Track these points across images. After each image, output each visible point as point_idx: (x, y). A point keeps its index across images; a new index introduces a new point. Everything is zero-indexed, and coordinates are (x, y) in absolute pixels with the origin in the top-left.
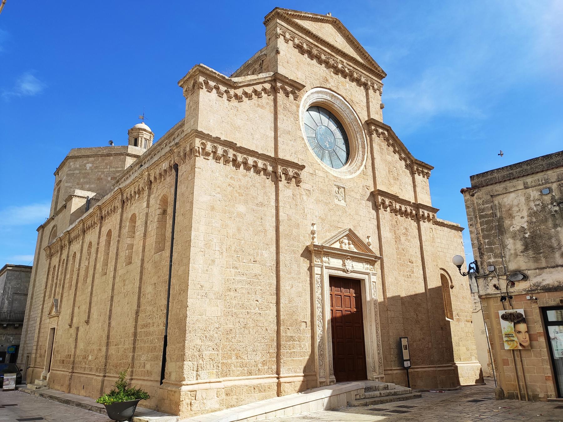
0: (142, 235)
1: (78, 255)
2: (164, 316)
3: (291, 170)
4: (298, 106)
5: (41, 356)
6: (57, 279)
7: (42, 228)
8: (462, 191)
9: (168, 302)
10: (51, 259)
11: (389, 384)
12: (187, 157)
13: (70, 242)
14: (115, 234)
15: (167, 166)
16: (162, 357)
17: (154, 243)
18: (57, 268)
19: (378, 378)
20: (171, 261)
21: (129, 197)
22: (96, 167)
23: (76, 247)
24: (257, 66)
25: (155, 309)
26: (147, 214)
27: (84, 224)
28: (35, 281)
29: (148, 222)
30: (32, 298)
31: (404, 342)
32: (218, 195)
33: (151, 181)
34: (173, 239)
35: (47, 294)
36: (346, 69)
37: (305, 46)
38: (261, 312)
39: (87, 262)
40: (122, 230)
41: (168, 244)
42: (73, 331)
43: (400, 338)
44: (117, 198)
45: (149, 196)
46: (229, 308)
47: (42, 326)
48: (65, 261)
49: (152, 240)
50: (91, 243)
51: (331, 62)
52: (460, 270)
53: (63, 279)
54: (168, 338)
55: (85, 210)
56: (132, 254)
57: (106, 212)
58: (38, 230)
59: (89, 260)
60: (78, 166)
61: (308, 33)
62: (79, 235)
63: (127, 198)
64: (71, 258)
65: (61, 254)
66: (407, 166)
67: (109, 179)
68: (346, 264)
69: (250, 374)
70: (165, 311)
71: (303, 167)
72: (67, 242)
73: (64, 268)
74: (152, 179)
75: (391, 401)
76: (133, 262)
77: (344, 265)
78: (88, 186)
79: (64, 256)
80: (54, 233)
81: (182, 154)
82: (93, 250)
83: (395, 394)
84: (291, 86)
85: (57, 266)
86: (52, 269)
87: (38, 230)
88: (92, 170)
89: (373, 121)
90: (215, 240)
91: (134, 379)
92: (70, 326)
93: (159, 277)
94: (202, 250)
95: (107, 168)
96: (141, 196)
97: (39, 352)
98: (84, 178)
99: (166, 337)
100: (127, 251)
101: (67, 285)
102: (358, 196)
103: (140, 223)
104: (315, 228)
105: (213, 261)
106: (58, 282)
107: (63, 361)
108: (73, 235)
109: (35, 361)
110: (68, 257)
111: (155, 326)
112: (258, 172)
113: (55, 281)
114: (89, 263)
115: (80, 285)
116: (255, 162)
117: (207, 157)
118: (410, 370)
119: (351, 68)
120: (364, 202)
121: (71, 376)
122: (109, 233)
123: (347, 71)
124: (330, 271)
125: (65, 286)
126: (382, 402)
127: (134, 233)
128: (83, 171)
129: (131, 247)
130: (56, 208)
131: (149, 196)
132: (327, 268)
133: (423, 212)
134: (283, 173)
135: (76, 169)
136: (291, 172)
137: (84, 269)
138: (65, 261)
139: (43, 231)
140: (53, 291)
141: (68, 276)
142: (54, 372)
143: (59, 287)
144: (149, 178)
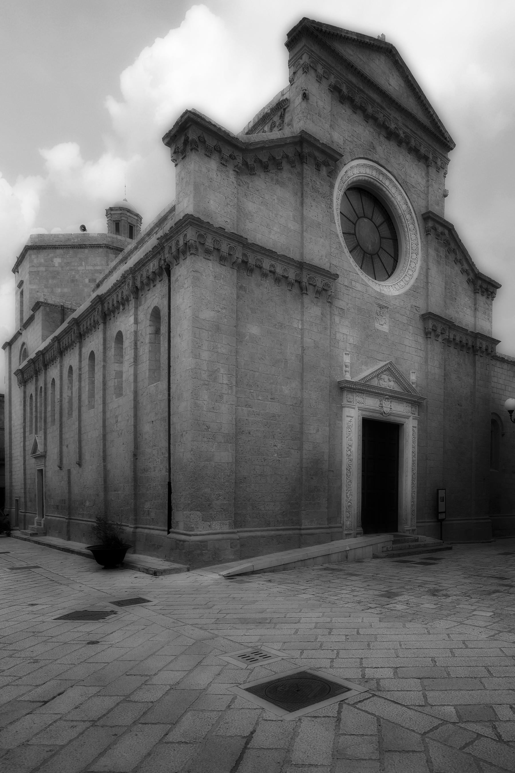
0: (132, 360)
1: (57, 382)
2: (166, 460)
3: (320, 280)
4: (332, 186)
5: (31, 501)
6: (36, 411)
7: (8, 345)
9: (169, 444)
10: (25, 386)
11: (420, 536)
12: (181, 255)
14: (99, 356)
15: (156, 267)
16: (167, 505)
17: (147, 372)
18: (34, 398)
19: (409, 530)
20: (169, 395)
21: (111, 309)
22: (68, 264)
23: (54, 372)
24: (276, 119)
25: (155, 452)
26: (136, 332)
27: (59, 343)
28: (10, 413)
29: (138, 343)
30: (10, 433)
31: (442, 493)
32: (224, 311)
33: (137, 287)
34: (169, 367)
35: (27, 429)
36: (401, 132)
37: (344, 89)
38: (280, 459)
39: (70, 392)
40: (108, 352)
41: (165, 372)
42: (64, 473)
43: (438, 490)
44: (97, 310)
46: (242, 454)
47: (27, 466)
48: (43, 389)
49: (145, 366)
50: (71, 368)
51: (381, 117)
52: (511, 416)
53: (43, 411)
54: (172, 485)
55: (59, 324)
56: (122, 384)
57: (85, 327)
58: (4, 347)
59: (71, 389)
60: (42, 261)
61: (350, 67)
63: (109, 309)
64: (49, 386)
65: (37, 380)
66: (469, 281)
67: (87, 281)
69: (268, 525)
70: (167, 455)
72: (41, 365)
73: (43, 398)
74: (139, 285)
75: (420, 553)
76: (124, 393)
78: (59, 290)
79: (41, 384)
80: (24, 353)
81: (174, 250)
82: (75, 376)
83: (425, 546)
84: (323, 152)
85: (34, 395)
86: (28, 399)
87: (4, 347)
88: (62, 267)
89: (431, 215)
90: (222, 371)
91: (139, 527)
92: (60, 468)
93: (156, 414)
94: (206, 383)
95: (81, 265)
96: (126, 307)
97: (28, 495)
98: (53, 278)
99: (169, 484)
100: (116, 380)
101: (49, 420)
102: (405, 320)
103: (128, 343)
105: (221, 396)
106: (38, 415)
107: (58, 506)
108: (48, 357)
109: (26, 506)
110: (45, 384)
111: (156, 471)
112: (277, 280)
113: (34, 413)
114: (72, 393)
115: (65, 419)
116: (272, 266)
117: (207, 257)
118: (444, 523)
119: (408, 131)
120: (411, 327)
121: (69, 523)
122: (92, 355)
123: (402, 135)
125: (48, 421)
126: (409, 554)
127: (122, 356)
128: (51, 269)
129: (119, 374)
130: (22, 319)
133: (481, 343)
134: (310, 284)
135: (40, 265)
136: (319, 282)
137: (67, 400)
138: (43, 389)
139: (10, 349)
140: (34, 426)
141: (49, 408)
142: (49, 518)
143: (40, 421)
144: (134, 283)
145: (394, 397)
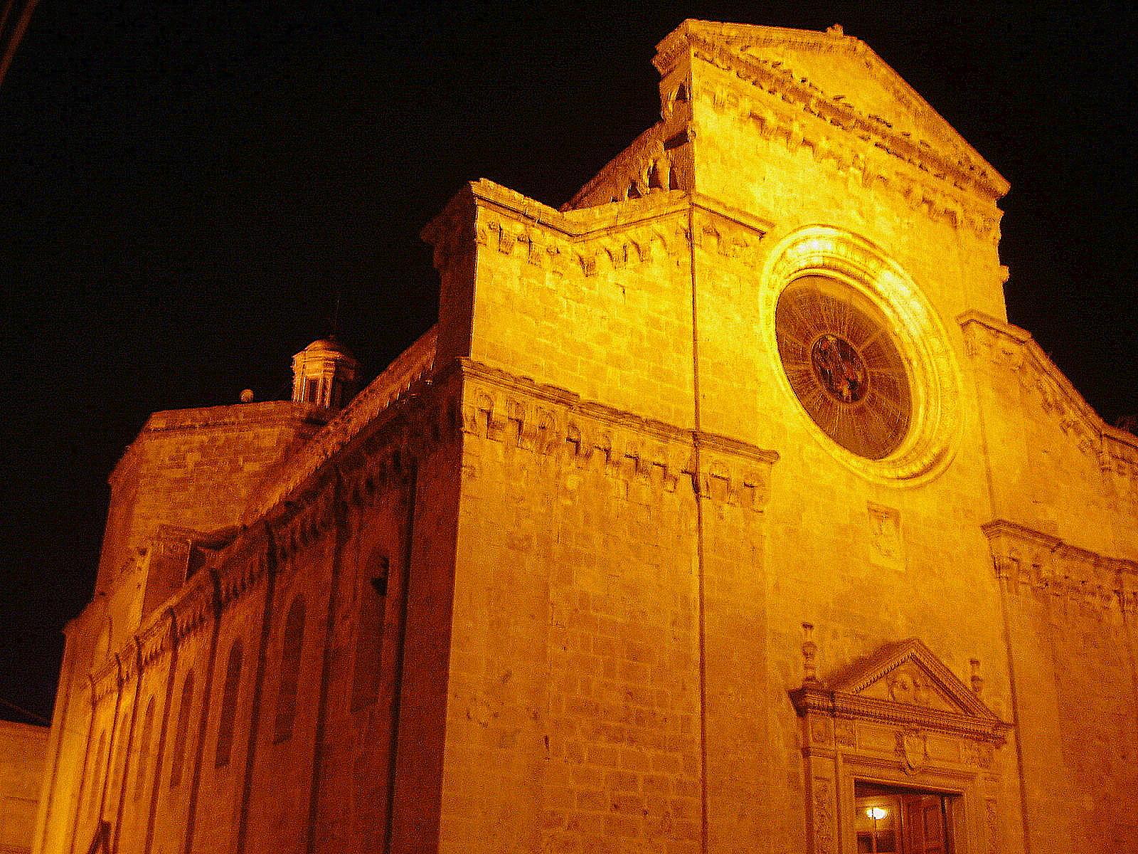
8: (984, 527)
13: (140, 670)
33: (122, 680)
45: (338, 552)
48: (130, 719)
62: (202, 620)
68: (907, 747)
71: (771, 456)
77: (900, 750)
104: (812, 636)
124: (858, 769)
131: (338, 552)
132: (847, 760)
145: (915, 721)
